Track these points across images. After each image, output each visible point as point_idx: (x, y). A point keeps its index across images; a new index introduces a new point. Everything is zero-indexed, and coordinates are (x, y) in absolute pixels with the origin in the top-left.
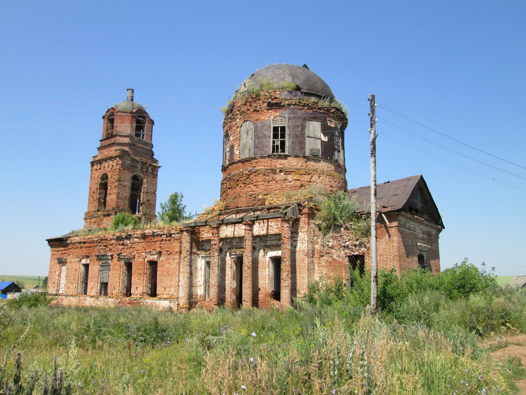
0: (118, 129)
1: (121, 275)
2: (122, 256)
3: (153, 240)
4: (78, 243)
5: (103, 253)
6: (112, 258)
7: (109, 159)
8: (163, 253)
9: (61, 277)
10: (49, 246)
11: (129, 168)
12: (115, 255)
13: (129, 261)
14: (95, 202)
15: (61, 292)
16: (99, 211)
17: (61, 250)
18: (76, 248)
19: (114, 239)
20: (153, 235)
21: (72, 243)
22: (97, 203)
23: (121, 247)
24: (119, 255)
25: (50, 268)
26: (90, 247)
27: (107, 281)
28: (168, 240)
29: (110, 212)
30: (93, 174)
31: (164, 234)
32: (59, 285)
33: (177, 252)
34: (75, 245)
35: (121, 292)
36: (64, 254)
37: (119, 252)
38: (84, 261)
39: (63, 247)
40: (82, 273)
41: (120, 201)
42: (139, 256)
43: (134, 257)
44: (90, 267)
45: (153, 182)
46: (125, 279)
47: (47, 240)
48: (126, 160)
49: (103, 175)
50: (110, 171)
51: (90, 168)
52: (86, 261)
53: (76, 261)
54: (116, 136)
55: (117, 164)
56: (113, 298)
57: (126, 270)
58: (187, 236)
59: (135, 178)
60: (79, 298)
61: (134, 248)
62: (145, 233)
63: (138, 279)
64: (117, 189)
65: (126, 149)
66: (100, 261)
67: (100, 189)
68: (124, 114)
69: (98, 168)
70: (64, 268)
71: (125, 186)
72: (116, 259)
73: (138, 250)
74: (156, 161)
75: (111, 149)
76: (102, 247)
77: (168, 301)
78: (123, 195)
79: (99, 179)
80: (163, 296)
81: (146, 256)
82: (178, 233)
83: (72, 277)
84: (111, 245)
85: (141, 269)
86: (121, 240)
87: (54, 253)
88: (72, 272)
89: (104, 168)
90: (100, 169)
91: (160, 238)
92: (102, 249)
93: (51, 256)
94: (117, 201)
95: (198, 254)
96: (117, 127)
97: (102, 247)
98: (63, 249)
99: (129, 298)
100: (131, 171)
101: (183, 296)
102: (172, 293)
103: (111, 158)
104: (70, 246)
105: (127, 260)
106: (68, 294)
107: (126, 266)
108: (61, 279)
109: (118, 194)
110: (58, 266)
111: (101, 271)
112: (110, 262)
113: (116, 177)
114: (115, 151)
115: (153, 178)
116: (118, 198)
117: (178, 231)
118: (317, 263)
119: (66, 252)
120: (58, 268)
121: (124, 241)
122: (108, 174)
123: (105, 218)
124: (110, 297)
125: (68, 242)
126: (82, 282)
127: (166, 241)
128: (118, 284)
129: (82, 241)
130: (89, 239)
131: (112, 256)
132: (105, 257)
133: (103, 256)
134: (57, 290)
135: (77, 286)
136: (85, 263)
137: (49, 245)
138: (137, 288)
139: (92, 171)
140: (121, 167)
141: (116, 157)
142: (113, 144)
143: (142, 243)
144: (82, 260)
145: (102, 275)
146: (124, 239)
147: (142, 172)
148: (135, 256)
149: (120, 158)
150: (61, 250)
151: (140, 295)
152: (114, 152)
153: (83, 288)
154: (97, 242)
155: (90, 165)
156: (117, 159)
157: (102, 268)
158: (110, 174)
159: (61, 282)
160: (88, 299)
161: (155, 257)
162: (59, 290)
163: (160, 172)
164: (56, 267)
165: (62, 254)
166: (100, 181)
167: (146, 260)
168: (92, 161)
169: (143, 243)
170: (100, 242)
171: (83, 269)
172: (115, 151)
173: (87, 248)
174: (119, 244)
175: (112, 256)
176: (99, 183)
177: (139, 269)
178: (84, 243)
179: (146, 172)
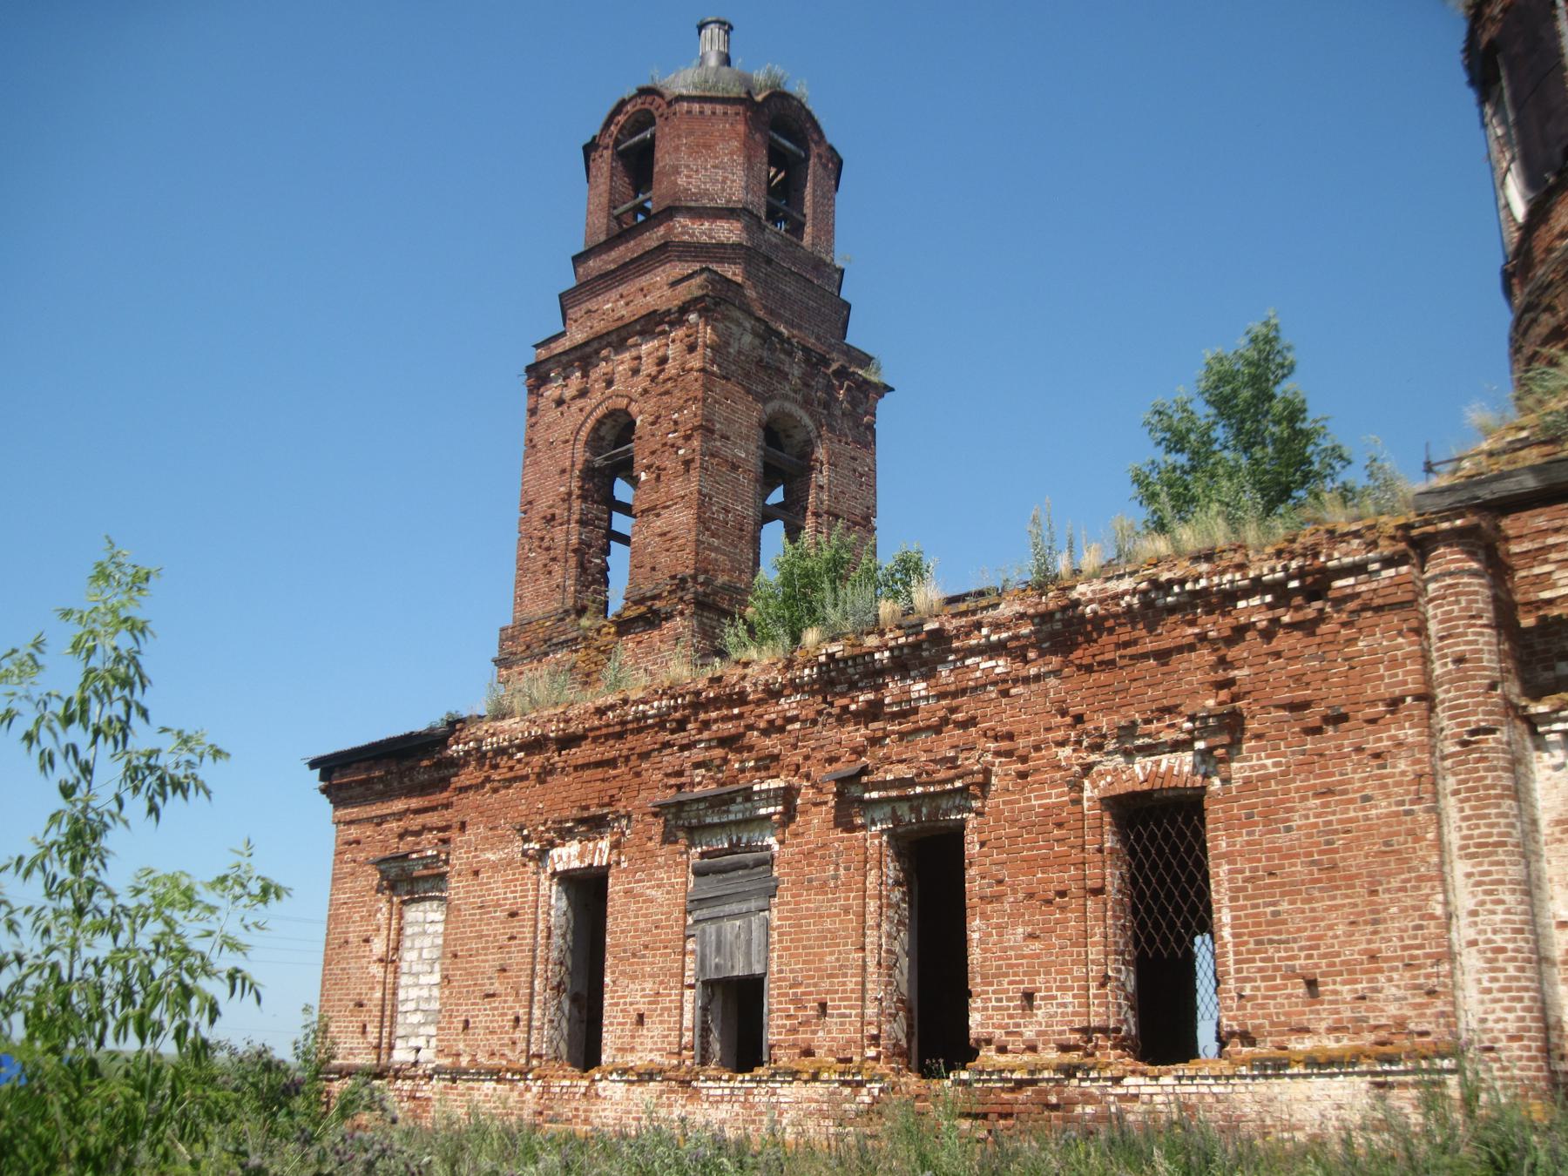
0: (681, 181)
1: (870, 922)
2: (884, 785)
3: (1149, 645)
4: (520, 748)
5: (703, 785)
6: (789, 815)
7: (642, 333)
8: (1253, 726)
9: (404, 966)
10: (324, 801)
11: (747, 375)
12: (807, 793)
13: (933, 814)
14: (556, 568)
15: (401, 1055)
16: (581, 611)
17: (399, 816)
18: (509, 782)
19: (796, 687)
20: (1147, 603)
21: (481, 757)
22: (573, 572)
23: (858, 734)
24: (844, 782)
25: (334, 918)
26: (612, 763)
27: (758, 969)
28: (1293, 626)
29: (658, 604)
30: (540, 428)
31: (1257, 587)
32: (388, 1012)
33: (1394, 703)
34: (503, 761)
35: (875, 1039)
36: (418, 833)
37: (844, 768)
38: (568, 856)
39: (409, 793)
40: (556, 932)
41: (716, 542)
42: (1023, 775)
43: (985, 786)
44: (615, 888)
45: (855, 465)
46: (897, 948)
47: (314, 764)
48: (734, 328)
49: (600, 422)
50: (645, 391)
51: (523, 400)
52: (581, 856)
53: (510, 863)
54: (669, 212)
55: (692, 348)
56: (815, 1077)
57: (897, 883)
58: (1474, 574)
59: (773, 434)
60: (546, 1089)
61: (971, 722)
62: (1076, 604)
63: (1032, 936)
64: (694, 474)
65: (733, 272)
66: (692, 845)
67: (583, 498)
68: (708, 108)
69: (568, 393)
70: (426, 919)
71: (734, 467)
72: (816, 821)
73: (1010, 736)
74: (866, 360)
75: (644, 281)
76: (698, 754)
77: (1362, 1084)
78: (727, 512)
79: (580, 446)
80: (1302, 1045)
81: (1087, 768)
82: (1388, 562)
83: (493, 959)
84: (771, 729)
85: (1062, 863)
86: (853, 686)
87: (354, 832)
88: (485, 930)
89: (610, 383)
90: (583, 393)
91: (1215, 626)
92: (697, 765)
93: (338, 853)
94: (698, 542)
95: (1532, 722)
96: (677, 172)
97: (698, 754)
98: (415, 803)
99: (965, 1075)
100: (760, 389)
101: (1512, 1027)
102: (1393, 1009)
103: (651, 324)
104: (465, 777)
105: (916, 810)
106: (464, 1061)
107: (899, 856)
108: (404, 980)
109: (704, 501)
110: (384, 906)
111: (700, 902)
112: (771, 841)
113: (690, 415)
114: (674, 284)
115: (856, 441)
116: (702, 521)
117: (1386, 548)
118: (1072, 911)
119: (433, 819)
120: (381, 918)
121: (878, 688)
122: (634, 408)
123: (629, 642)
124: (794, 1075)
125: (456, 749)
126: (558, 988)
127: (1268, 634)
128: (852, 983)
129: (553, 730)
130: (601, 712)
131: (787, 796)
132: (736, 812)
133: (719, 802)
134: (378, 1047)
135: (522, 1012)
136: (576, 864)
137: (324, 791)
138: (1029, 997)
139: (533, 412)
140: (713, 362)
141: (684, 309)
142: (663, 252)
143: (1038, 678)
144: (554, 852)
145: (711, 929)
146: (883, 672)
147: (807, 403)
148: (987, 772)
149: (705, 313)
150: (399, 816)
151: (1064, 1048)
152: (668, 292)
153: (564, 1024)
154: (661, 725)
155: (520, 384)
156: (693, 317)
157: (712, 887)
158: (650, 405)
159: (402, 995)
160: (613, 1089)
161: (1181, 765)
162: (391, 1047)
163: (885, 408)
164: (372, 914)
165: (401, 836)
166: (581, 454)
167: (1089, 792)
168: (532, 361)
169: (1052, 681)
170: (681, 725)
171: (556, 902)
172: (674, 284)
173: (587, 774)
174: (843, 717)
175: (787, 796)
176: (579, 466)
177: (1031, 864)
178: (567, 741)
179: (826, 406)
